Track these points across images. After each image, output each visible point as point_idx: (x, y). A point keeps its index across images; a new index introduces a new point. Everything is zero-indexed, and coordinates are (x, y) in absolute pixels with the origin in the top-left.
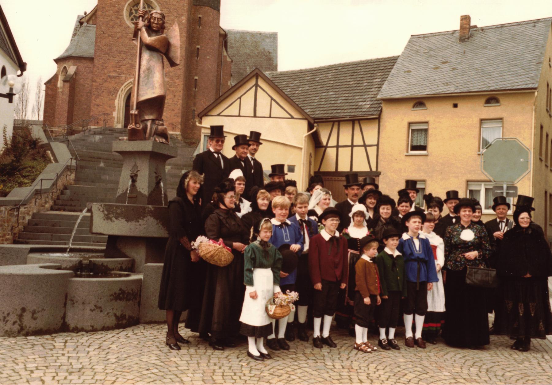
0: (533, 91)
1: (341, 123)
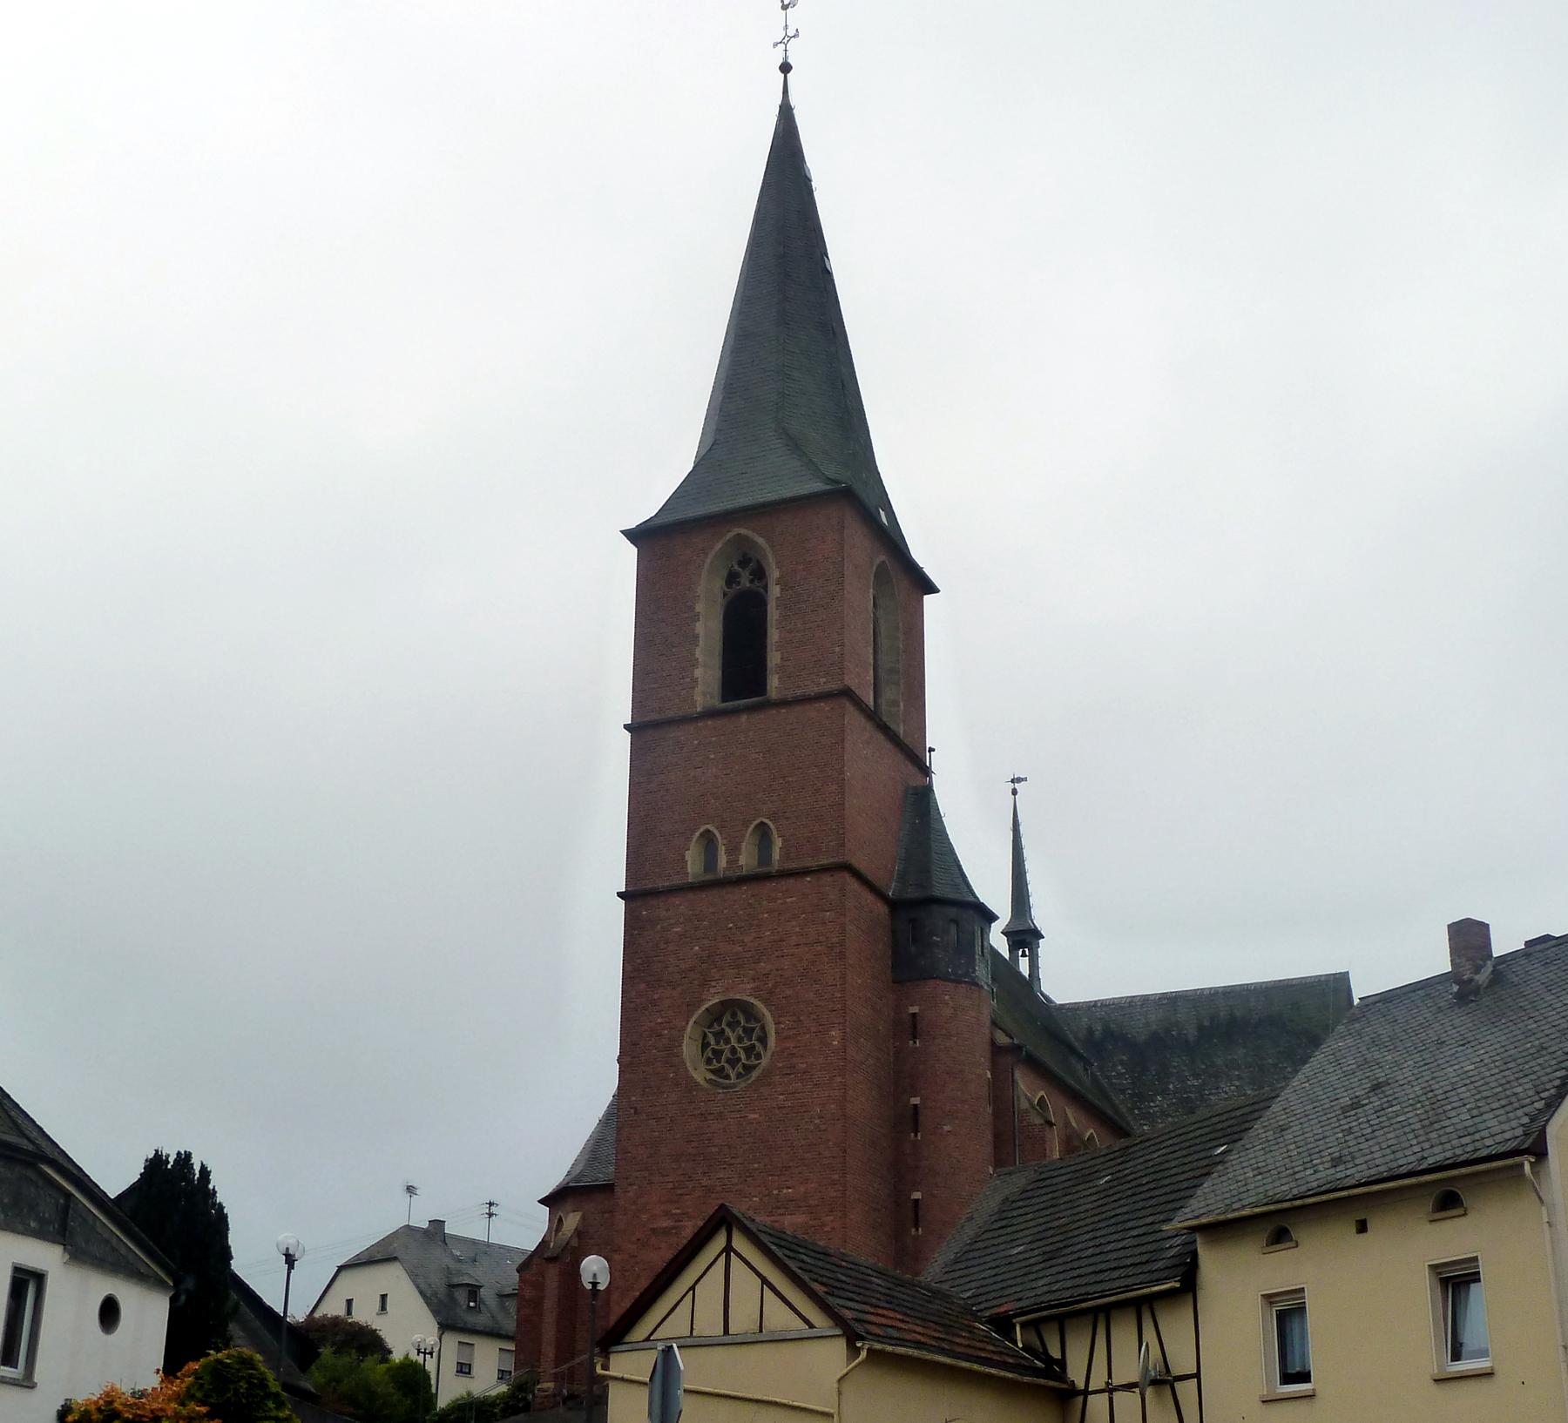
0: (1518, 1159)
1: (1115, 1314)
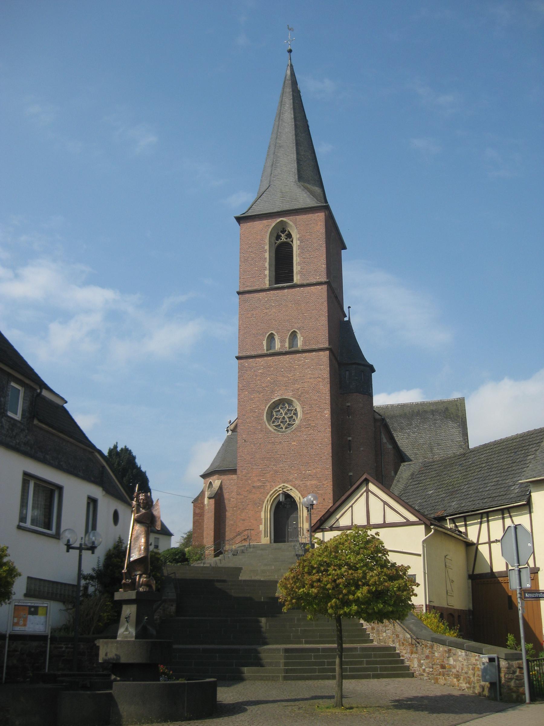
1: (490, 514)
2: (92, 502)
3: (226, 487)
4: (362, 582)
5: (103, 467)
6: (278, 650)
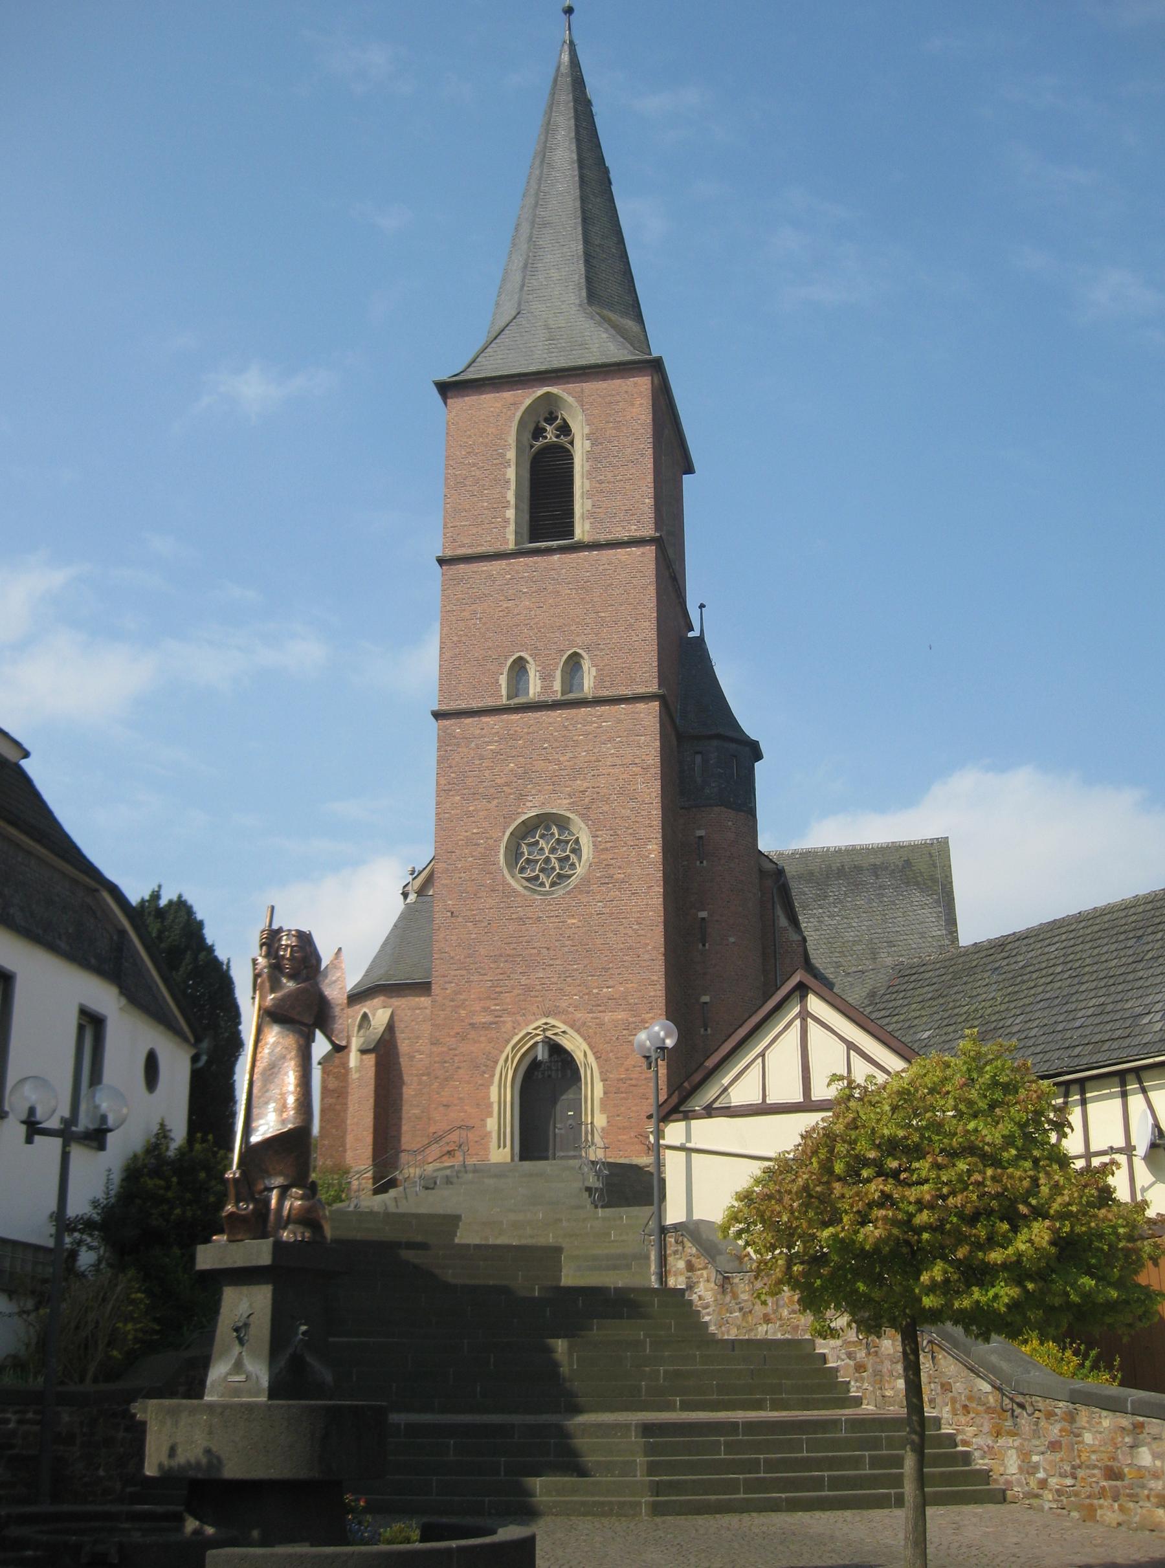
1: (1088, 1085)
2: (92, 1024)
3: (403, 1025)
4: (1029, 1205)
5: (122, 933)
6: (626, 1427)
